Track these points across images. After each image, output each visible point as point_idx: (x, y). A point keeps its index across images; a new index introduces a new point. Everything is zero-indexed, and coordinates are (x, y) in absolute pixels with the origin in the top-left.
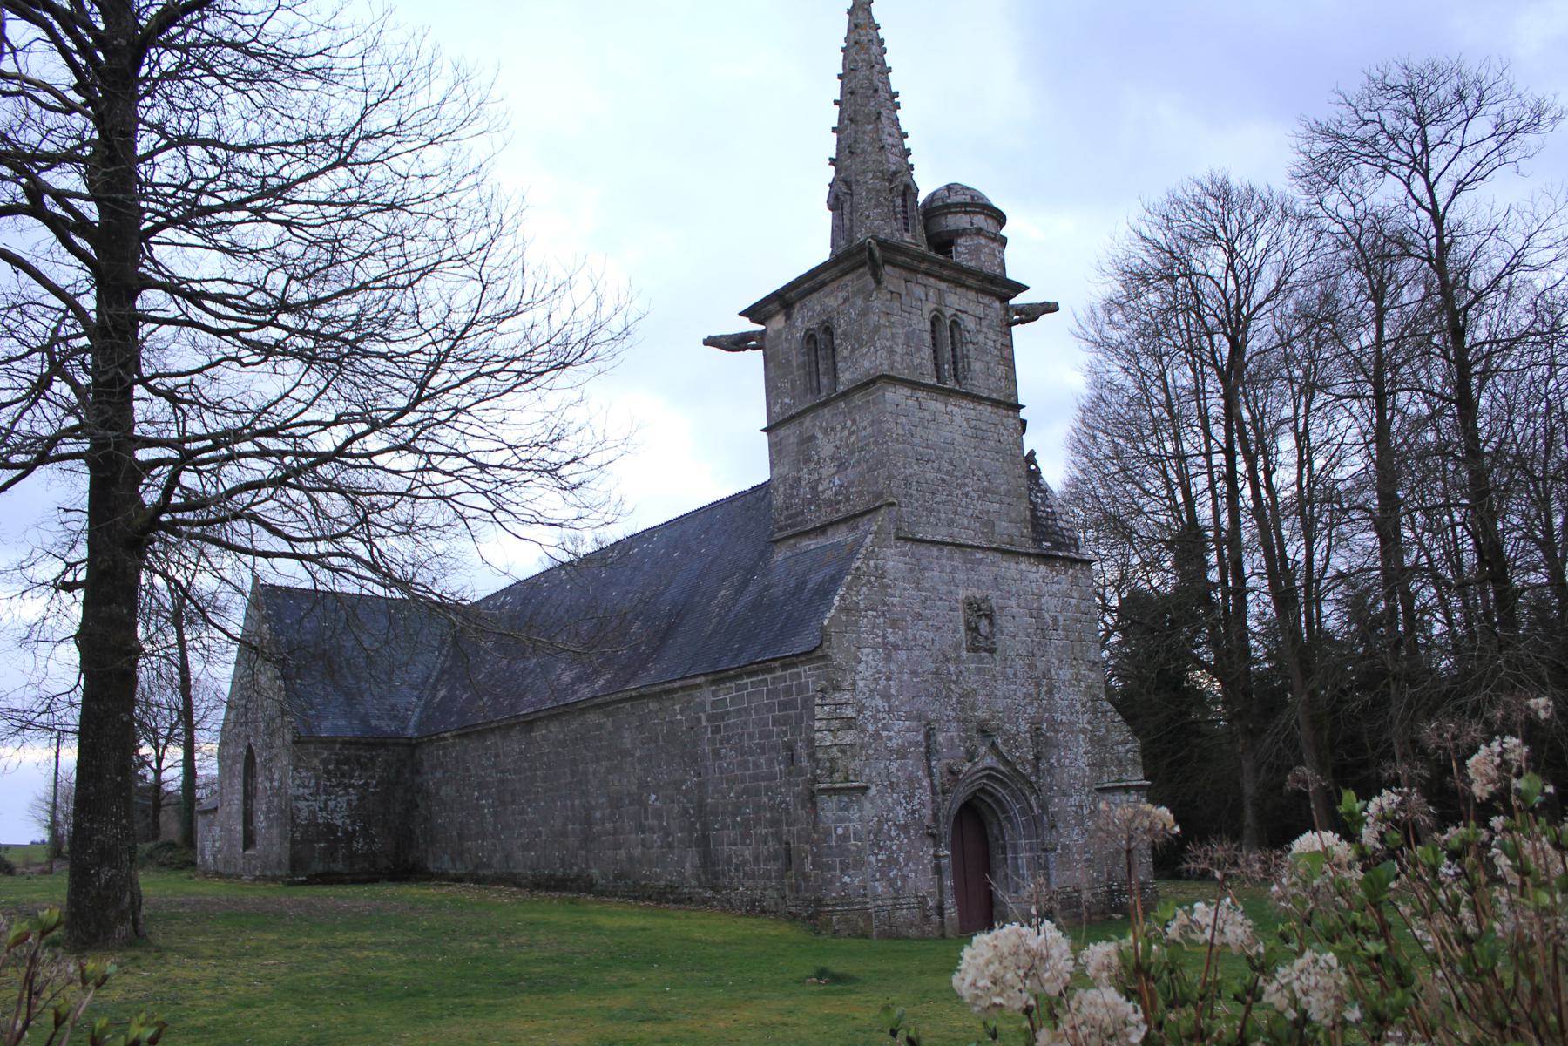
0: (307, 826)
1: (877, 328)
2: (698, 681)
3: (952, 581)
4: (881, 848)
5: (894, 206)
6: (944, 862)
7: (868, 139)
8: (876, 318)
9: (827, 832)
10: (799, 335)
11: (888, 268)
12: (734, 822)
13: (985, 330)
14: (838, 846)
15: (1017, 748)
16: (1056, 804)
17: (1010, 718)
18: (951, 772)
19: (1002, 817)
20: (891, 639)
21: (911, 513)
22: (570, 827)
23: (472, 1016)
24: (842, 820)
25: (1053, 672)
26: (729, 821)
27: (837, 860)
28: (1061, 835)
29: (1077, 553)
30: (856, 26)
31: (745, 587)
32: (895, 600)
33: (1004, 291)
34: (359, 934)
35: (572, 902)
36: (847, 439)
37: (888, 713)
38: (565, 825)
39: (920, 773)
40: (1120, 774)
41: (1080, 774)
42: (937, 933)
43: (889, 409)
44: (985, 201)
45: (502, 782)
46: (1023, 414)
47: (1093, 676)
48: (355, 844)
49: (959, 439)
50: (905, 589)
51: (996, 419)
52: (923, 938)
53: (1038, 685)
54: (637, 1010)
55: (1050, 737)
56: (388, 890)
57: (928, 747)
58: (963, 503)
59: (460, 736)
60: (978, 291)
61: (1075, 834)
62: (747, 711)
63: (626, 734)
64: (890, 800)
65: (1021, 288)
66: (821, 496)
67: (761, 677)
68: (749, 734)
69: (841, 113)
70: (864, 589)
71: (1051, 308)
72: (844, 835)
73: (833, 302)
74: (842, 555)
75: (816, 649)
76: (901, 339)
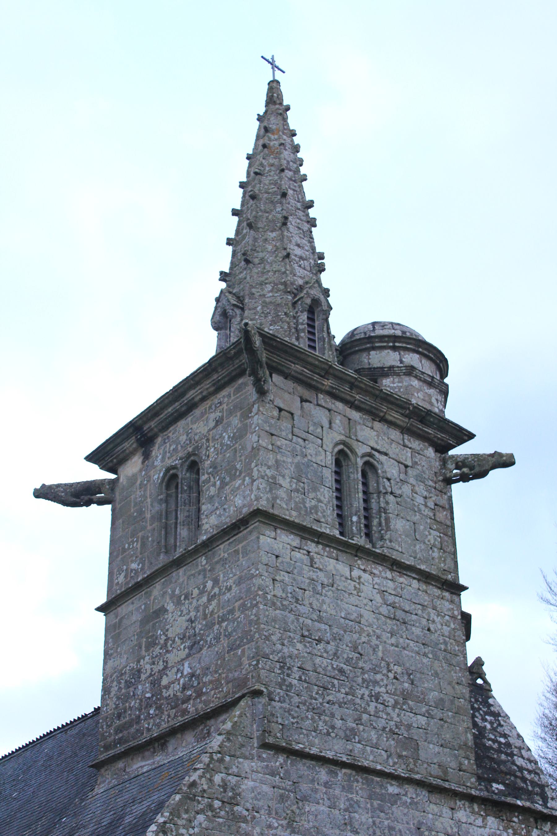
5: (297, 324)
8: (255, 438)
10: (157, 476)
13: (412, 480)
21: (289, 711)
29: (545, 805)
36: (206, 607)
43: (265, 559)
44: (420, 338)
49: (368, 616)
50: (270, 827)
51: (425, 599)
58: (372, 708)
60: (404, 430)
66: (165, 694)
70: (201, 818)
76: (289, 471)
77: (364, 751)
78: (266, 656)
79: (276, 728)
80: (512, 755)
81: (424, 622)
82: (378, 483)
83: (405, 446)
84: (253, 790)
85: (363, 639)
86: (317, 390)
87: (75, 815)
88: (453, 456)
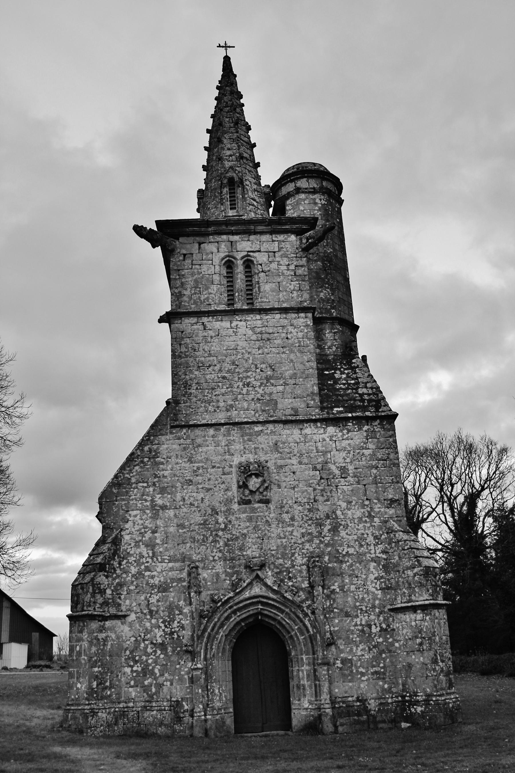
4: (136, 662)
14: (77, 659)
21: (190, 407)
25: (339, 513)
32: (166, 473)
37: (152, 558)
39: (182, 603)
49: (242, 344)
51: (285, 322)
60: (271, 233)
70: (137, 468)
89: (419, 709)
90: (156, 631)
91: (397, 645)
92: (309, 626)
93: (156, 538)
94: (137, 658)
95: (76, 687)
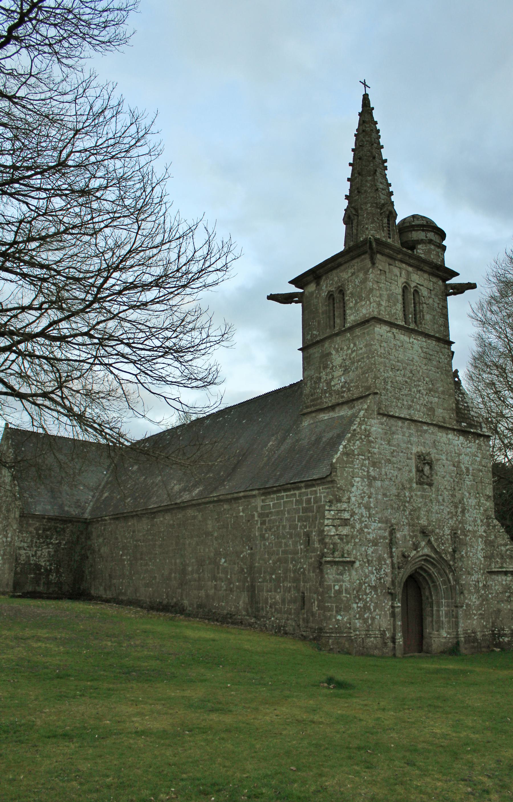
0: (24, 564)
1: (371, 290)
2: (254, 493)
3: (409, 442)
4: (360, 600)
5: (383, 223)
6: (398, 610)
7: (369, 185)
8: (371, 284)
9: (329, 588)
10: (324, 294)
11: (379, 256)
12: (271, 578)
13: (433, 296)
14: (335, 596)
15: (443, 544)
16: (464, 579)
17: (439, 526)
18: (404, 556)
19: (431, 585)
20: (372, 473)
21: (387, 399)
22: (173, 575)
23: (95, 698)
24: (337, 581)
25: (465, 500)
26: (268, 577)
27: (334, 605)
28: (465, 598)
29: (481, 430)
30: (364, 122)
31: (284, 440)
32: (376, 450)
33: (445, 275)
34: (40, 631)
35: (171, 619)
36: (350, 355)
37: (369, 518)
38: (170, 574)
39: (385, 555)
40: (502, 564)
41: (478, 562)
42: (391, 654)
45: (136, 546)
46: (453, 348)
47: (488, 504)
48: (51, 576)
49: (416, 358)
50: (381, 444)
52: (382, 656)
53: (456, 507)
54: (209, 701)
55: (462, 539)
56: (66, 604)
57: (391, 540)
58: (417, 396)
59: (114, 519)
61: (474, 598)
62: (282, 512)
63: (210, 522)
64: (367, 571)
65: (455, 274)
67: (292, 492)
68: (283, 526)
69: (353, 170)
70: (358, 442)
71: (472, 286)
72: (339, 590)
73: (345, 275)
74: (344, 423)
75: (327, 476)
76: (385, 297)
77: (415, 413)
78: (379, 378)
79: (383, 407)
80: (469, 411)
81: (437, 359)
82: (419, 299)
83: (430, 281)
84: (375, 431)
85: (415, 368)
86: (395, 259)
87: (296, 434)
88: (450, 284)
89: (506, 639)
90: (372, 576)
91: (490, 596)
92: (451, 579)
93: (370, 502)
94: (361, 597)
95: (336, 619)
